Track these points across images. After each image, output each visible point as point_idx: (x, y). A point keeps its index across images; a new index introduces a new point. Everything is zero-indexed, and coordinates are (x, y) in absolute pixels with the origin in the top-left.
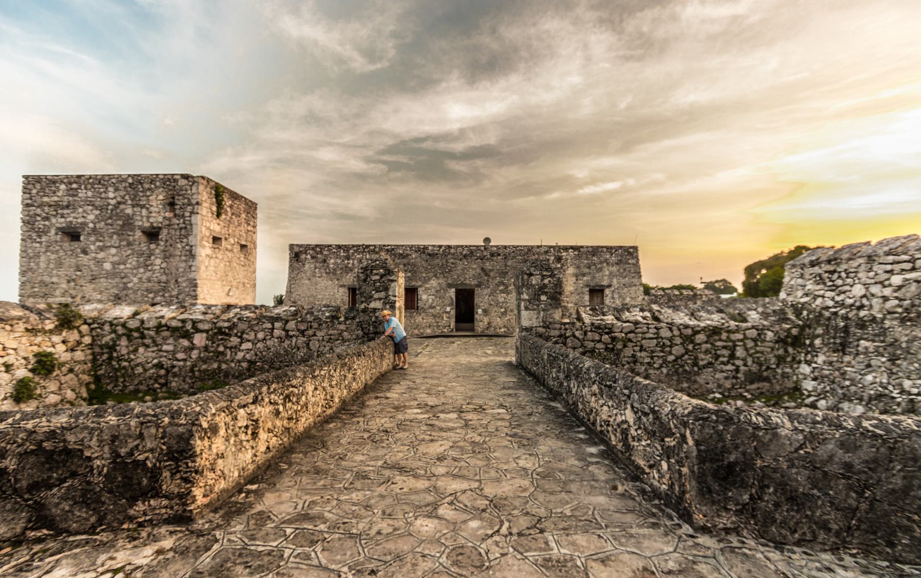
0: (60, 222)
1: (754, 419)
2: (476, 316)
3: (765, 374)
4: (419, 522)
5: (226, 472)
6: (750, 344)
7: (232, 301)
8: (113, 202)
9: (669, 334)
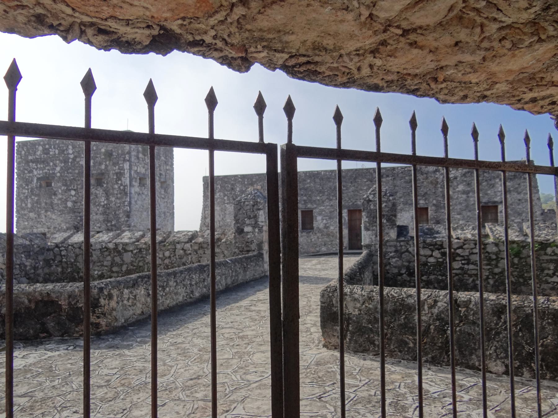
8: (72, 156)
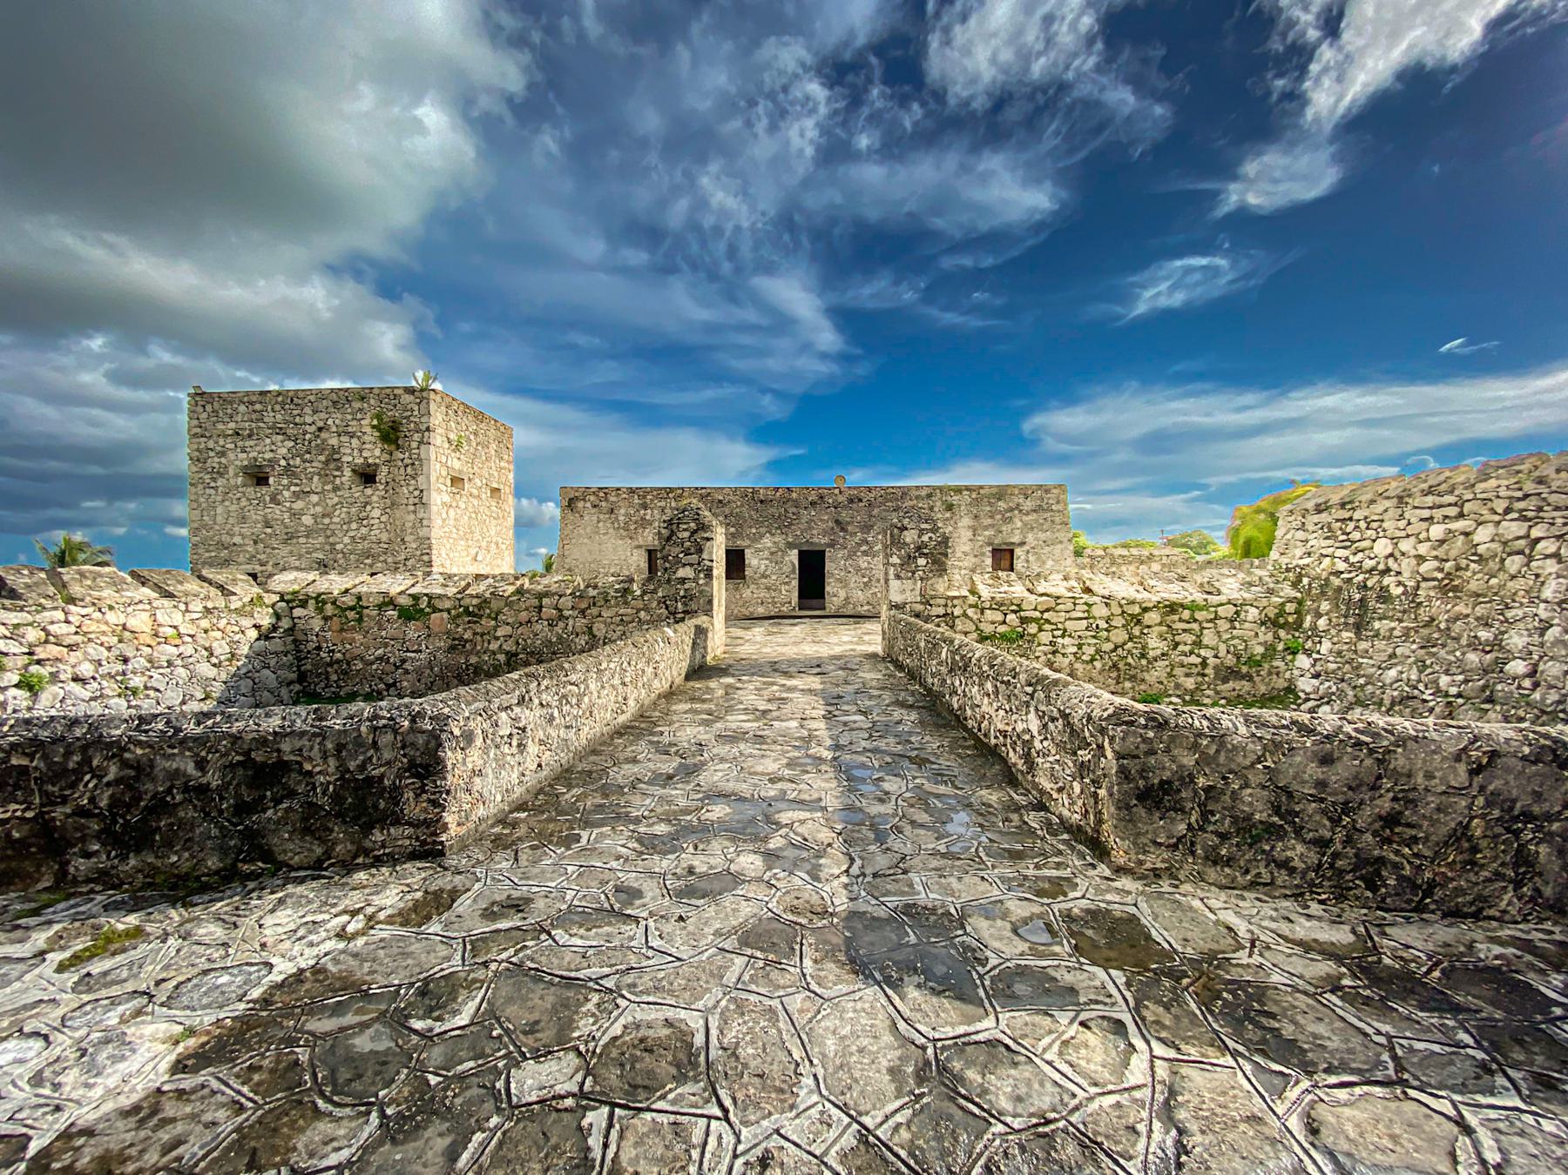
0: (243, 459)
1: (1197, 723)
2: (828, 588)
3: (1244, 669)
4: (742, 859)
5: (486, 794)
6: (1223, 625)
7: (483, 570)
9: (1105, 612)
